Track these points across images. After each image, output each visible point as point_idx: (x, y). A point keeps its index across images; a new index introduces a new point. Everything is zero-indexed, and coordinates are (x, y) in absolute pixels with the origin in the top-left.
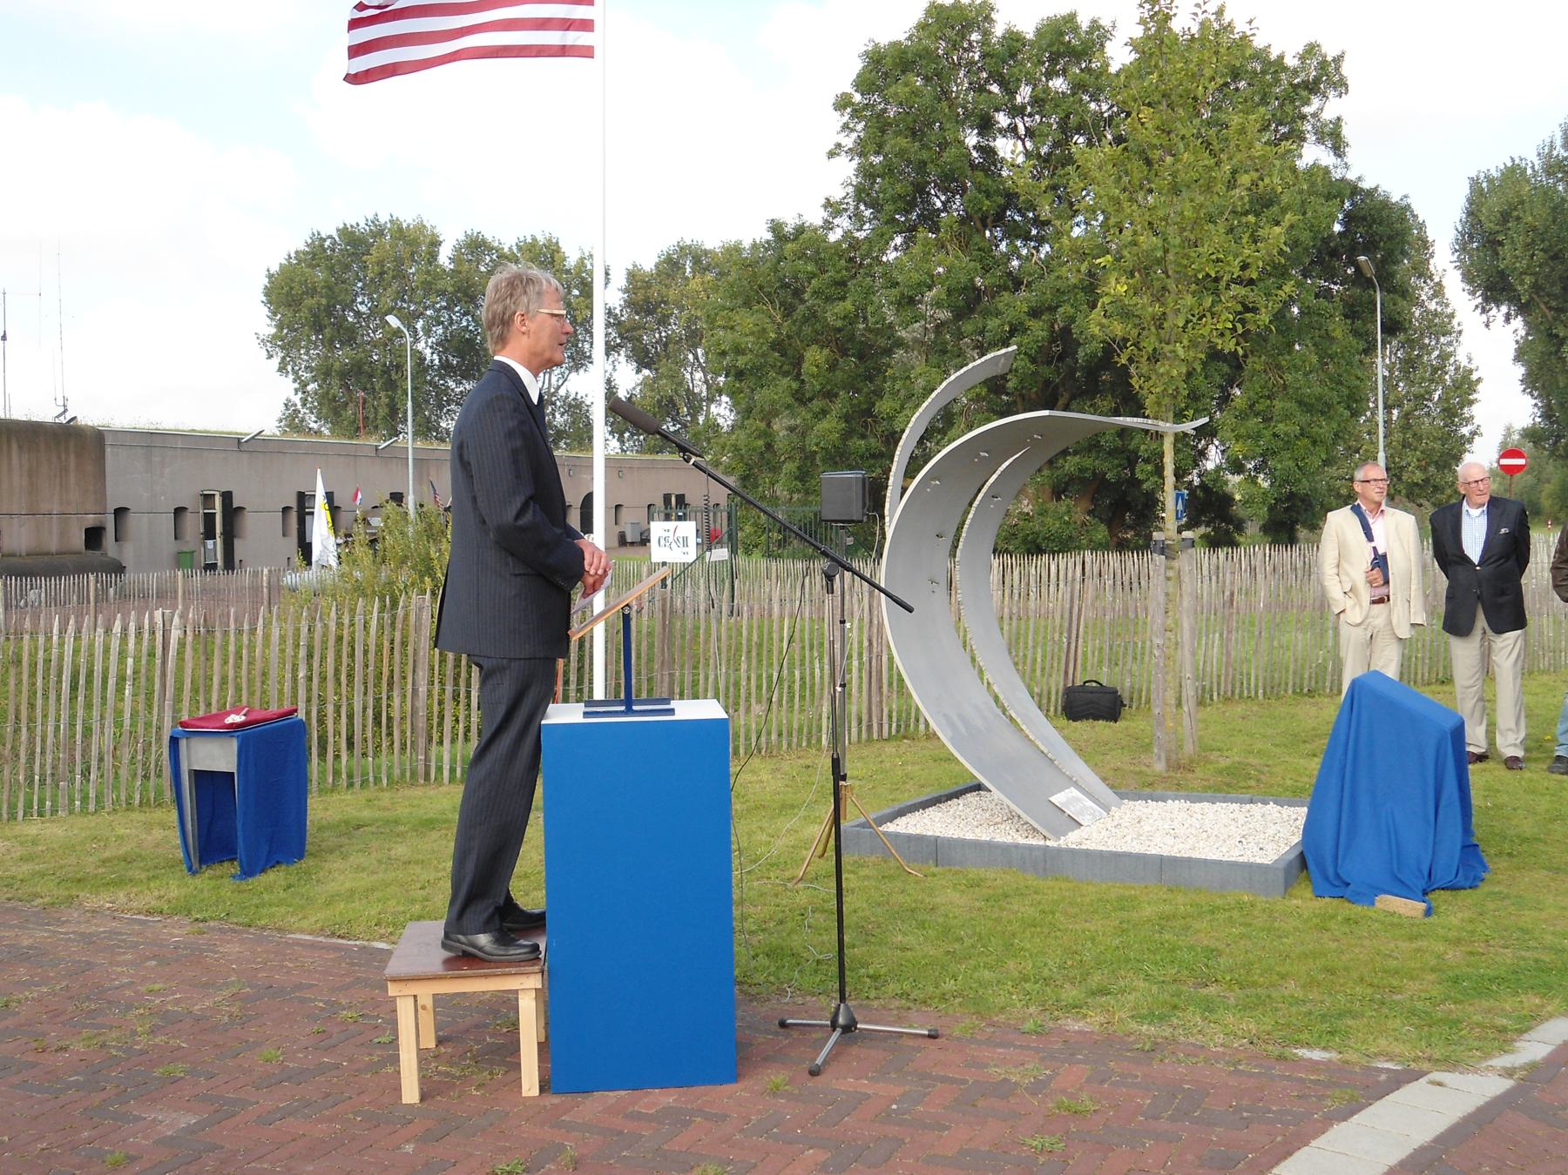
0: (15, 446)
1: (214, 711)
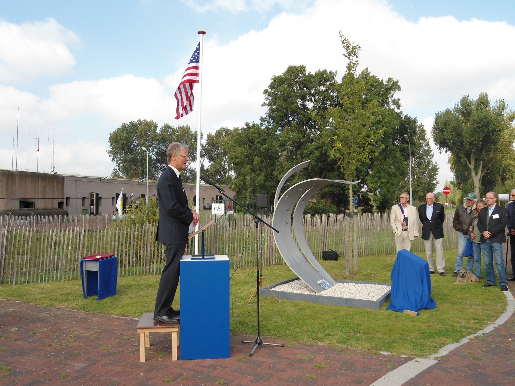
0: (40, 181)
1: (93, 254)
